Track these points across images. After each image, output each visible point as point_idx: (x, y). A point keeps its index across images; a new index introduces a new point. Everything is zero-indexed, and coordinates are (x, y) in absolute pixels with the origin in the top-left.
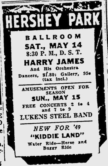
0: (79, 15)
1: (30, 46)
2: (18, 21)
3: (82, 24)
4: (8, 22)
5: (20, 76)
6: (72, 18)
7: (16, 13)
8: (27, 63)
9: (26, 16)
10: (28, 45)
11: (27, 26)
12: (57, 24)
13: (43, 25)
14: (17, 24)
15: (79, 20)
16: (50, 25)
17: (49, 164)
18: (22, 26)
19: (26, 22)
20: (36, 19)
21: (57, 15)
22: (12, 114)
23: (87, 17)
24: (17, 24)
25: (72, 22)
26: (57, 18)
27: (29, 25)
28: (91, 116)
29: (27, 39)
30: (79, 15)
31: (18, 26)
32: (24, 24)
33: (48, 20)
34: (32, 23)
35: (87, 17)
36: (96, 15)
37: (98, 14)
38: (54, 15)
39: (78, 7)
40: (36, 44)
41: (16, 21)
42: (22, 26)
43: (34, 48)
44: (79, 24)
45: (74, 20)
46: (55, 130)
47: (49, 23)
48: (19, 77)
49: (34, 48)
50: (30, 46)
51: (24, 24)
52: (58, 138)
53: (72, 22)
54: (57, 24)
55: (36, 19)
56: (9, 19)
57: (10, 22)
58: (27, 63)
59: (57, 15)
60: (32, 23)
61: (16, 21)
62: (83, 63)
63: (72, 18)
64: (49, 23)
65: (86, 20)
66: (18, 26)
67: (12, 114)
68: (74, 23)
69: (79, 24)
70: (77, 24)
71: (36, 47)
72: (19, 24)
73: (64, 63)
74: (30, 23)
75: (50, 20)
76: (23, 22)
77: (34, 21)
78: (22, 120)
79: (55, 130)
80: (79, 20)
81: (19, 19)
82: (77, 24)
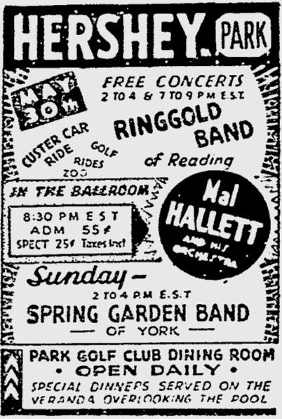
4: (19, 38)
7: (193, 237)
11: (88, 55)
14: (55, 47)
15: (188, 218)
16: (170, 54)
17: (176, 416)
18: (72, 56)
20: (116, 29)
21: (191, 20)
22: (62, 59)
24: (55, 47)
26: (191, 30)
28: (246, 318)
31: (58, 56)
33: (161, 36)
36: (213, 186)
38: (183, 18)
39: (191, 209)
42: (72, 56)
46: (190, 292)
47: (165, 46)
48: (145, 98)
52: (72, 151)
55: (116, 29)
56: (26, 30)
57: (32, 38)
59: (191, 20)
60: (106, 46)
61: (51, 38)
64: (165, 46)
66: (58, 56)
67: (62, 59)
72: (61, 47)
73: (120, 242)
74: (97, 43)
75: (167, 36)
76: (74, 40)
78: (94, 400)
79: (190, 292)
80: (188, 218)
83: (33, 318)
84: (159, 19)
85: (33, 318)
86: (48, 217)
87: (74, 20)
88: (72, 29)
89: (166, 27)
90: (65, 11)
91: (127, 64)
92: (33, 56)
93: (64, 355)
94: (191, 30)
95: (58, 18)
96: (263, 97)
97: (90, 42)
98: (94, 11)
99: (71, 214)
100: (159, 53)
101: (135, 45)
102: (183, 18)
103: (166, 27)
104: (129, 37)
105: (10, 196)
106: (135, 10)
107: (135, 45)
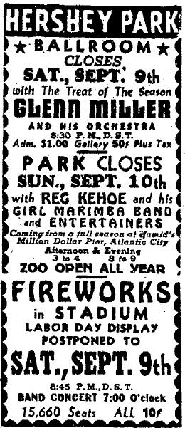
0: (140, 14)
1: (35, 74)
2: (28, 20)
3: (145, 31)
4: (9, 20)
5: (21, 397)
6: (127, 18)
8: (101, 197)
9: (45, 12)
10: (31, 69)
11: (46, 29)
12: (105, 30)
13: (77, 29)
15: (140, 25)
18: (38, 29)
19: (44, 23)
21: (105, 14)
23: (42, 18)
24: (28, 25)
25: (126, 26)
26: (105, 19)
27: (50, 29)
29: (39, 48)
30: (140, 14)
32: (156, 28)
34: (57, 26)
35: (42, 18)
37: (175, 13)
38: (100, 13)
40: (49, 70)
41: (26, 20)
42: (38, 29)
43: (44, 79)
44: (140, 31)
45: (130, 22)
47: (89, 26)
49: (44, 79)
50: (35, 74)
51: (156, 28)
53: (126, 26)
54: (105, 30)
57: (76, 21)
58: (101, 197)
59: (105, 14)
60: (57, 26)
61: (86, 22)
62: (19, 175)
63: (127, 18)
64: (89, 26)
65: (153, 24)
68: (130, 28)
69: (140, 31)
70: (135, 31)
71: (48, 75)
72: (32, 24)
77: (59, 22)
80: (140, 25)
81: (32, 16)
82: (135, 31)
83: (157, 160)
84: (86, 13)
85: (157, 160)
86: (68, 136)
87: (39, 12)
88: (38, 17)
89: (89, 17)
90: (34, 7)
91: (180, 15)
92: (16, 28)
93: (144, 291)
94: (105, 19)
95: (30, 11)
96: (115, 117)
97: (47, 24)
98: (50, 8)
99: (113, 124)
100: (86, 30)
101: (73, 25)
102: (100, 13)
103: (89, 17)
104: (70, 21)
105: (108, 88)
106: (73, 8)
107: (73, 25)
